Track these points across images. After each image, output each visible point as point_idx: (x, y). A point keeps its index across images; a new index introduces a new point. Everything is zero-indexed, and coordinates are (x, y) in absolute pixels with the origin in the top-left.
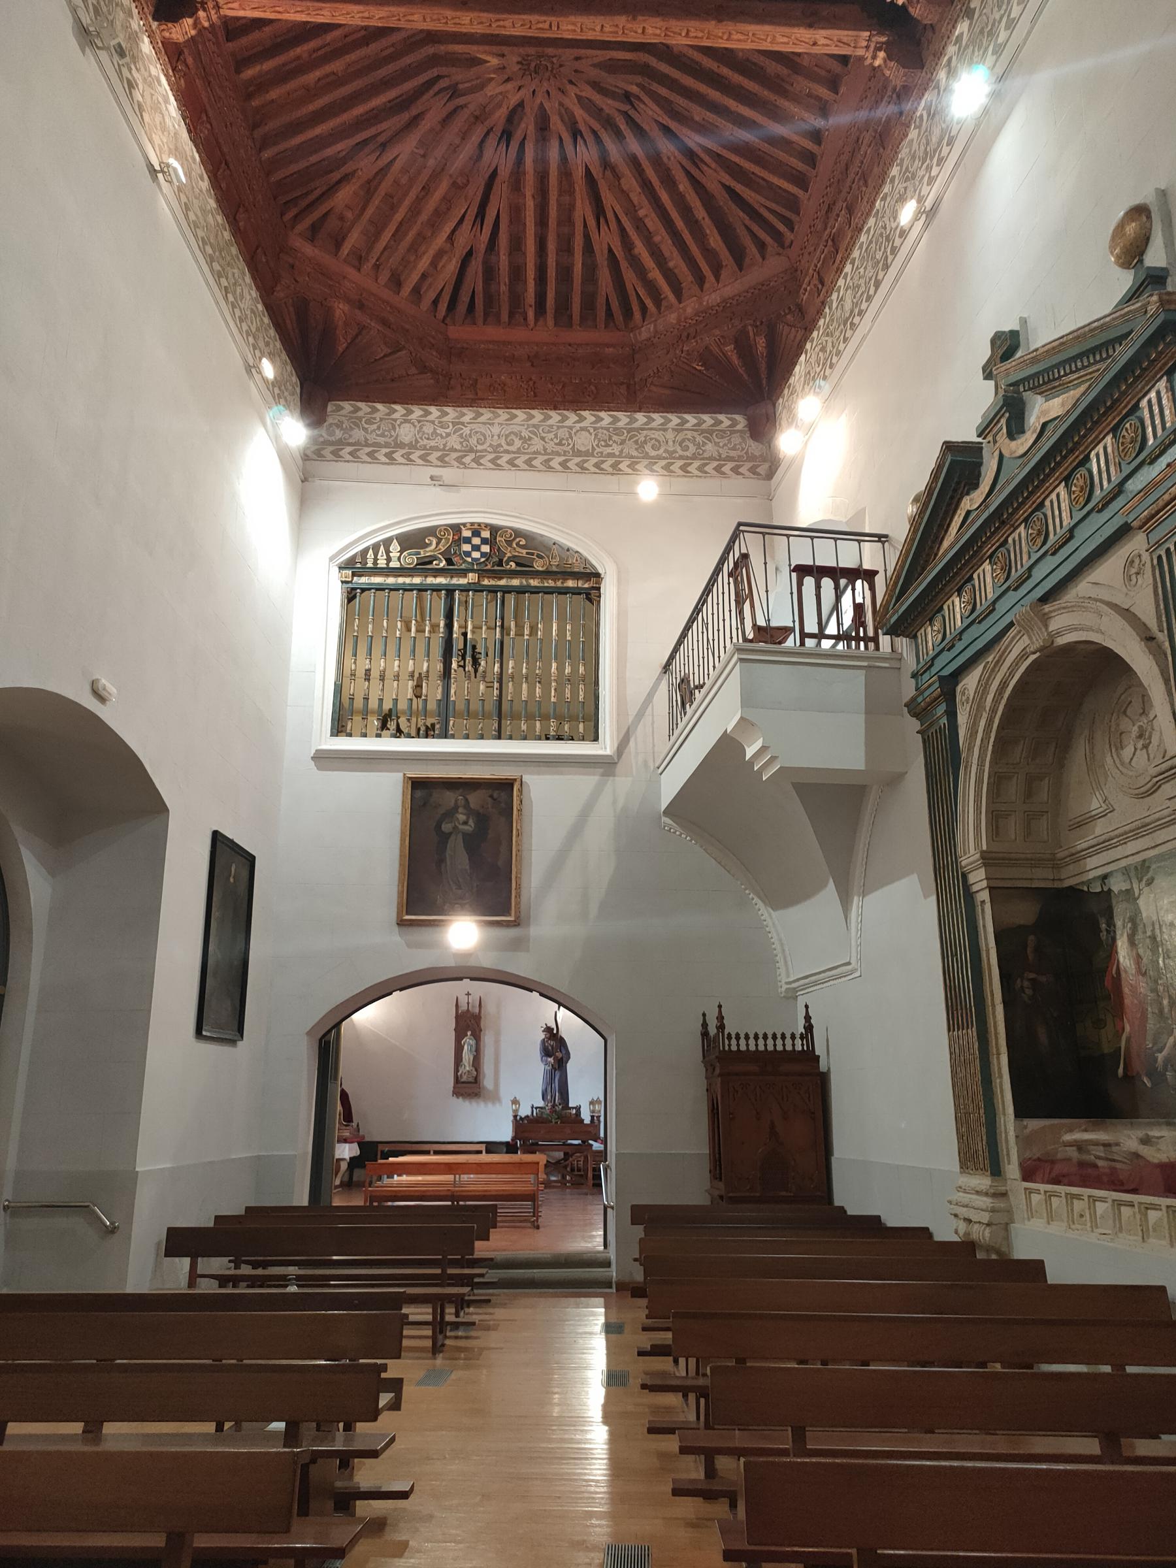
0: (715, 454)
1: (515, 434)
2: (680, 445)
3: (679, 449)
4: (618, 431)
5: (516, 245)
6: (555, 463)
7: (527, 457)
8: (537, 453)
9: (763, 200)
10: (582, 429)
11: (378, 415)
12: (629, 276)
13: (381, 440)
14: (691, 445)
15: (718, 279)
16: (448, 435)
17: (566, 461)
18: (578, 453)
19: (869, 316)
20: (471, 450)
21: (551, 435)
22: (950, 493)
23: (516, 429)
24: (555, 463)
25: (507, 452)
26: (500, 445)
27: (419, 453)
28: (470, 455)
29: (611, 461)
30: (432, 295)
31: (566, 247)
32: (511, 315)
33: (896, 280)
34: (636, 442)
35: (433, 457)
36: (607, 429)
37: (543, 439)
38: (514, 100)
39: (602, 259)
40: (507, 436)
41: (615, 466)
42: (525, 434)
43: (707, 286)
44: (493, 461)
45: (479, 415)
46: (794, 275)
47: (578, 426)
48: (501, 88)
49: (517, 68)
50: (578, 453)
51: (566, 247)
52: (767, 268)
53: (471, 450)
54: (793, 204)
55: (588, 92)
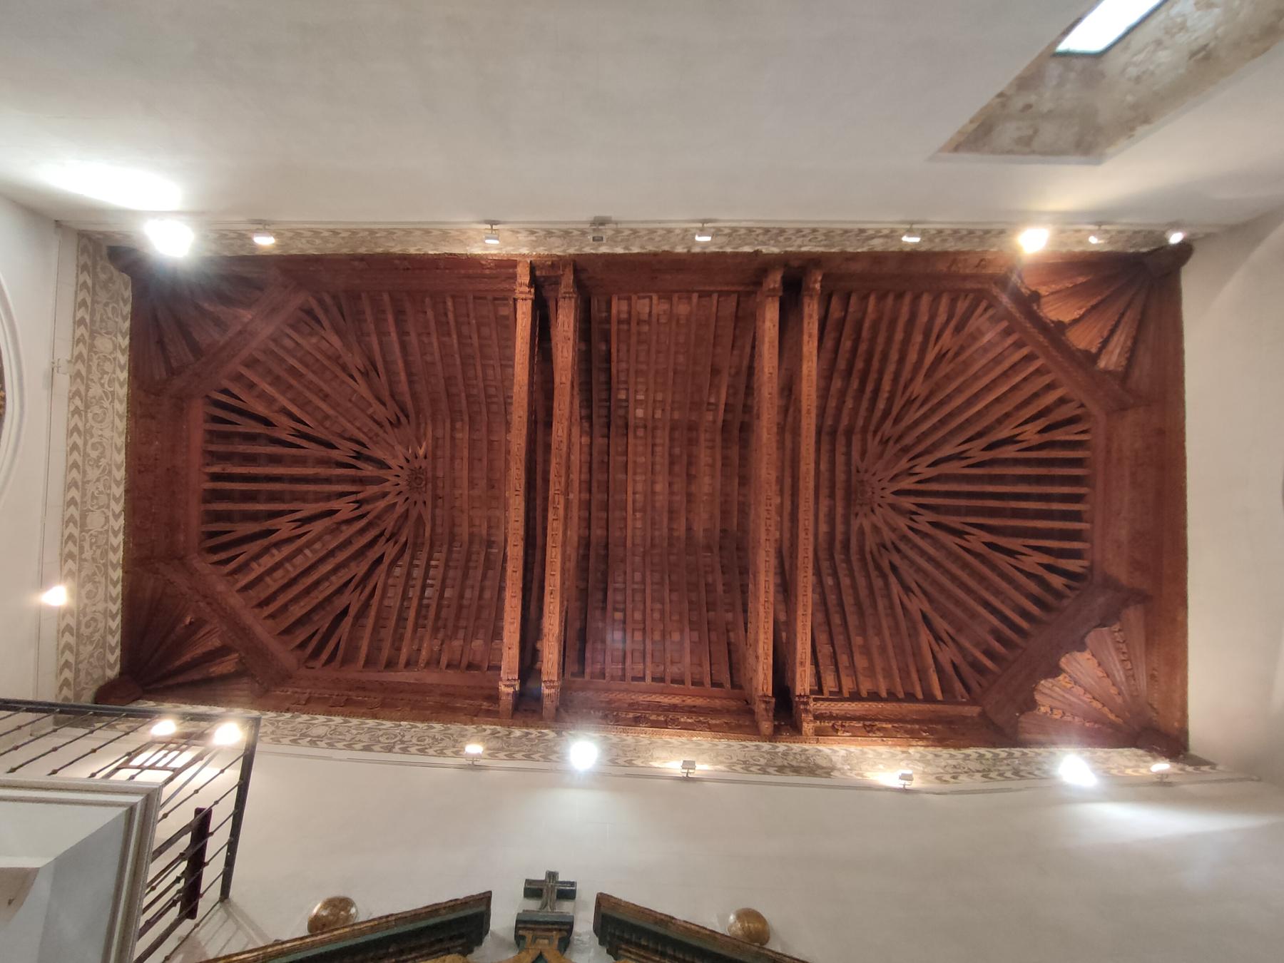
0: (81, 658)
1: (103, 453)
2: (93, 619)
3: (88, 618)
4: (104, 554)
5: (275, 460)
6: (74, 493)
7: (80, 464)
8: (85, 472)
9: (344, 638)
10: (107, 518)
11: (119, 320)
12: (255, 547)
13: (98, 317)
14: (91, 629)
15: (266, 618)
16: (102, 385)
17: (76, 504)
18: (84, 516)
19: (279, 748)
20: (87, 407)
21: (101, 488)
22: (456, 933)
23: (108, 453)
24: (74, 493)
25: (85, 444)
26: (92, 436)
27: (85, 352)
28: (81, 404)
29: (75, 550)
30: (236, 391)
31: (273, 497)
32: (211, 453)
33: (401, 763)
34: (94, 574)
35: (81, 367)
36: (106, 543)
37: (98, 480)
38: (391, 462)
39: (268, 524)
40: (100, 443)
41: (70, 556)
42: (103, 462)
43: (257, 611)
44: (76, 429)
45: (120, 417)
46: (285, 678)
47: (110, 514)
48: (401, 456)
49: (417, 466)
50: (84, 516)
51: (273, 497)
52: (284, 654)
53: (87, 407)
54: (348, 660)
55: (400, 510)
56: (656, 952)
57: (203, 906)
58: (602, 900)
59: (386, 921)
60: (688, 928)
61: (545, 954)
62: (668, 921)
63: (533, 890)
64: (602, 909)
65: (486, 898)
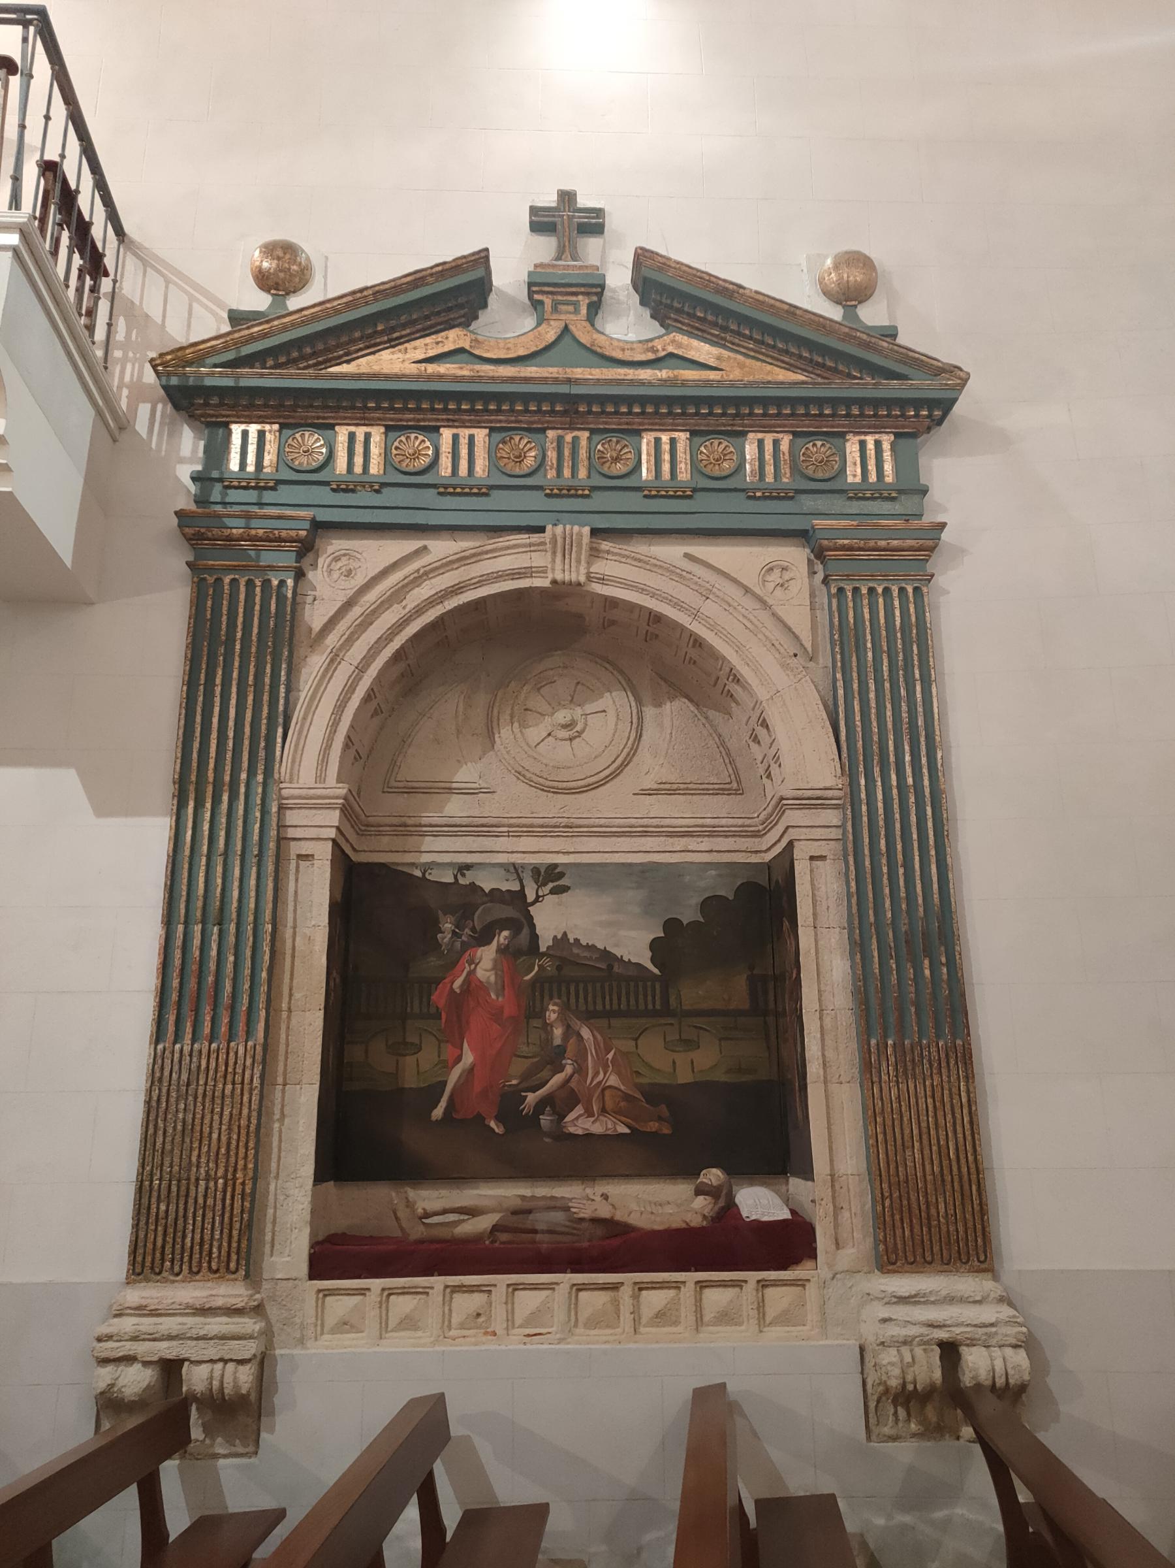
56: (715, 325)
57: (109, 262)
58: (643, 257)
59: (358, 297)
60: (762, 302)
61: (571, 327)
62: (732, 290)
63: (542, 222)
64: (646, 272)
65: (481, 259)
